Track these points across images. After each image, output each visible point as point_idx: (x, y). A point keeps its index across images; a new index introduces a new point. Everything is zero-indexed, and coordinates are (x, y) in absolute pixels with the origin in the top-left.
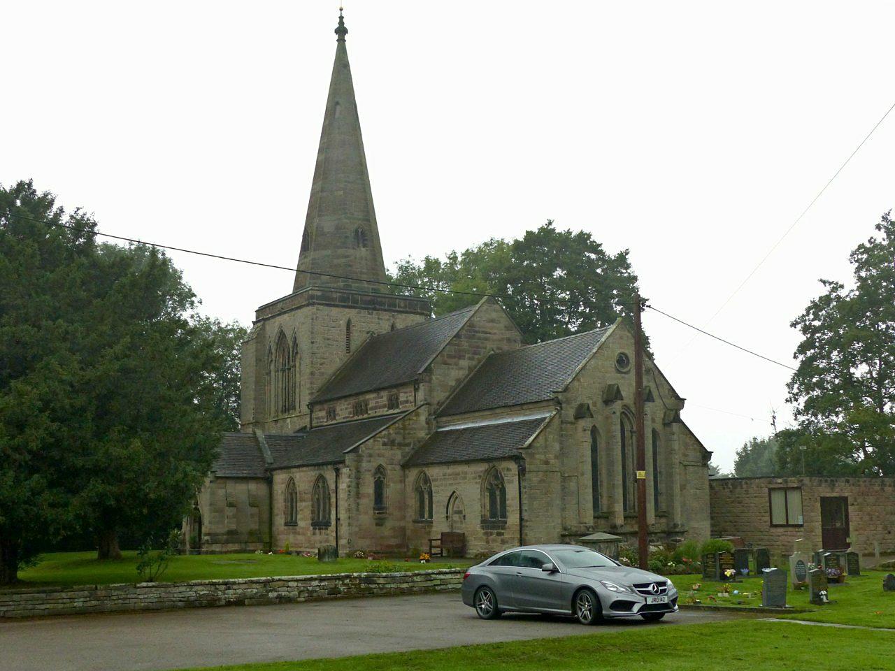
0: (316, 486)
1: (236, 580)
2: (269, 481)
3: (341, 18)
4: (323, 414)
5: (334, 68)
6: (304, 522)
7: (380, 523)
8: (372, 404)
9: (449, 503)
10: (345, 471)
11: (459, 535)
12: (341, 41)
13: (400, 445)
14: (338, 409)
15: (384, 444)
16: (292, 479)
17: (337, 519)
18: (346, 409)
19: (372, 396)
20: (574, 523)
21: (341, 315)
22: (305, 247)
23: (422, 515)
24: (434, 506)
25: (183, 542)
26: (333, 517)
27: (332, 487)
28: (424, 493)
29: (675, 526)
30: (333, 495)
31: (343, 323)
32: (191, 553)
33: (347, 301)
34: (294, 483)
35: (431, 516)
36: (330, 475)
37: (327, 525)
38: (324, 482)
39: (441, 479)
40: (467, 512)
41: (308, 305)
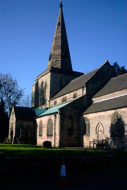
0: (48, 123)
1: (10, 130)
3: (61, 3)
5: (71, 64)
8: (68, 98)
9: (98, 125)
18: (60, 101)
24: (91, 129)
26: (54, 132)
27: (54, 122)
30: (54, 125)
34: (42, 122)
35: (89, 133)
37: (52, 135)
38: (51, 121)
39: (93, 119)
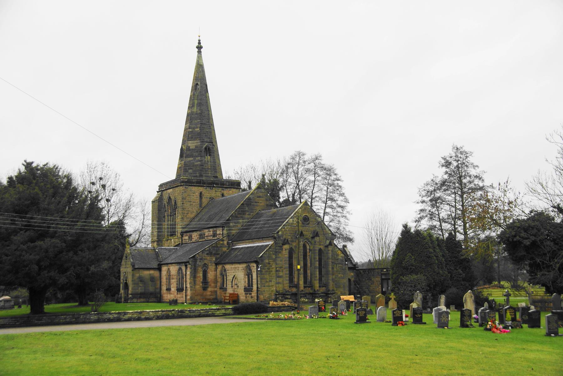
2: (159, 269)
4: (187, 238)
6: (173, 289)
7: (205, 289)
10: (189, 266)
11: (236, 294)
12: (199, 52)
13: (215, 254)
14: (193, 236)
15: (207, 254)
16: (169, 269)
17: (186, 287)
19: (206, 231)
20: (281, 289)
21: (197, 190)
22: (181, 156)
23: (224, 286)
25: (121, 298)
27: (184, 273)
28: (224, 274)
29: (329, 291)
31: (198, 194)
32: (124, 302)
33: (200, 183)
36: (183, 268)
40: (239, 284)
41: (181, 185)
